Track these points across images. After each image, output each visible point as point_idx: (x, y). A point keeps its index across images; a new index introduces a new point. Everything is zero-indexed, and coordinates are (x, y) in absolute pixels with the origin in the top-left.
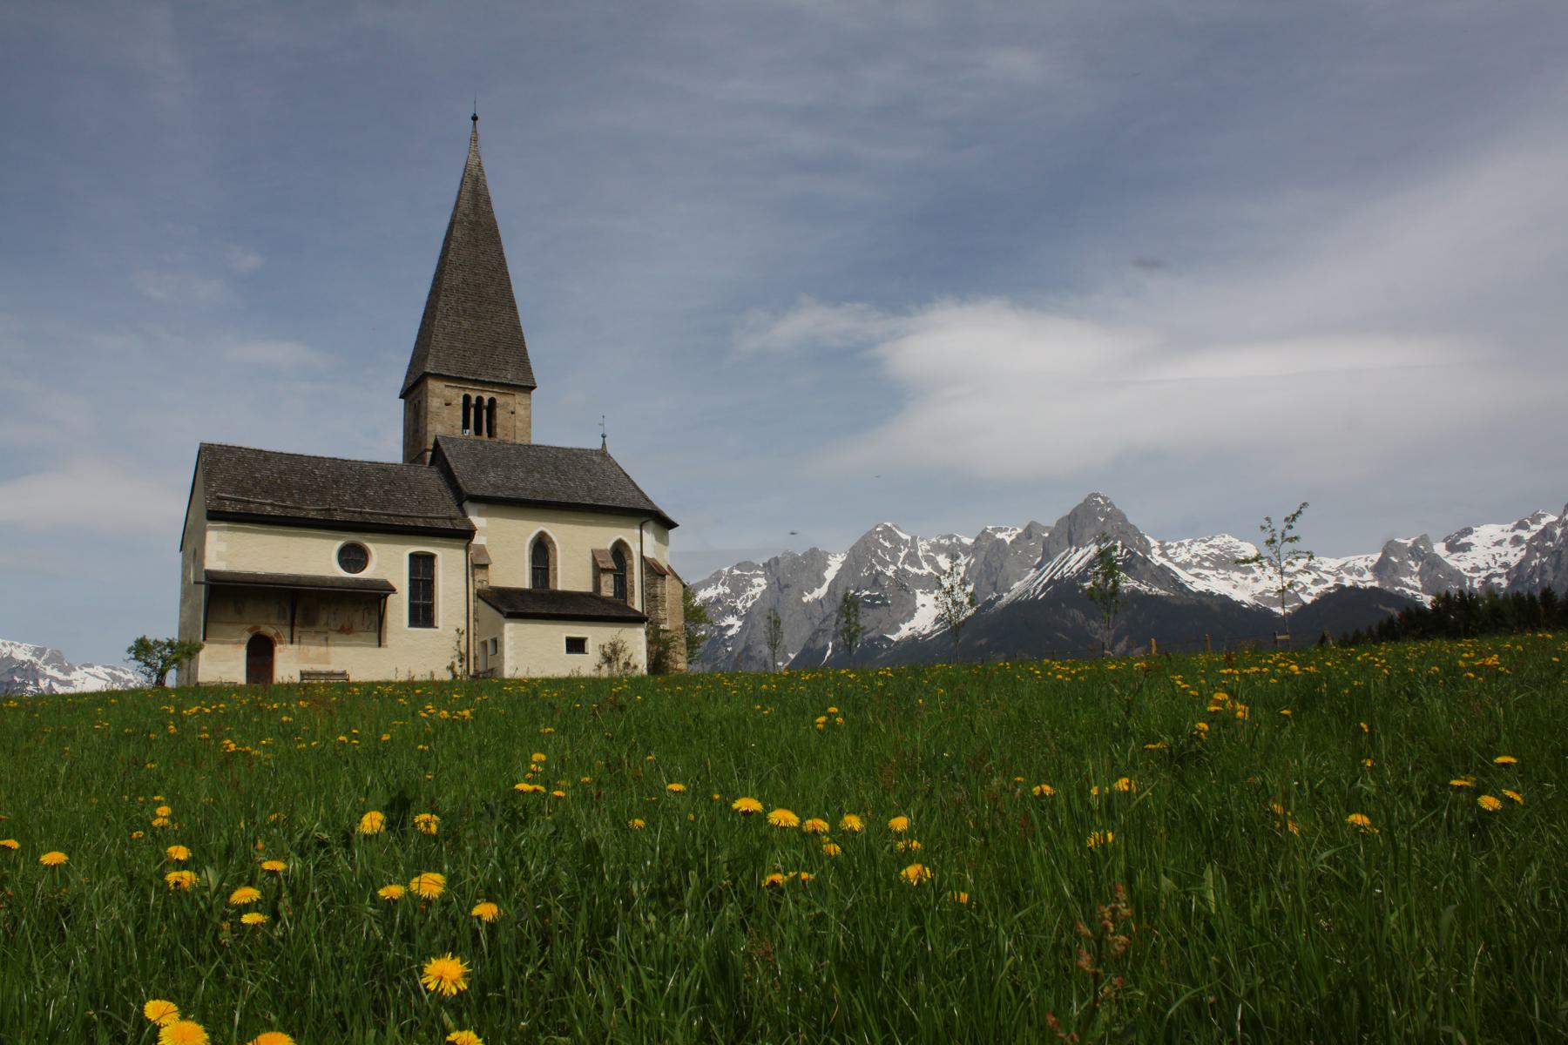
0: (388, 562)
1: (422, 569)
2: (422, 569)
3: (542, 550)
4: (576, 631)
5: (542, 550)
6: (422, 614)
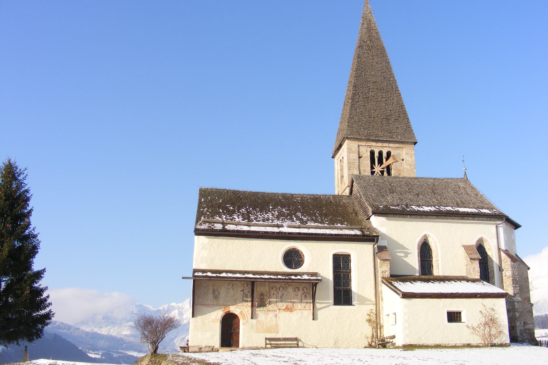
0: (318, 259)
1: (341, 264)
2: (341, 264)
3: (425, 250)
4: (454, 305)
5: (425, 250)
6: (343, 296)
